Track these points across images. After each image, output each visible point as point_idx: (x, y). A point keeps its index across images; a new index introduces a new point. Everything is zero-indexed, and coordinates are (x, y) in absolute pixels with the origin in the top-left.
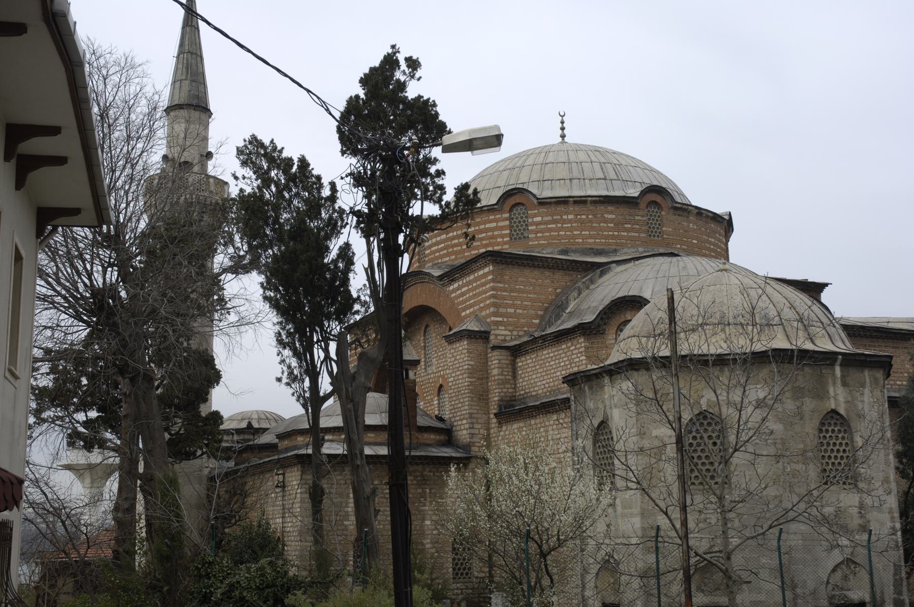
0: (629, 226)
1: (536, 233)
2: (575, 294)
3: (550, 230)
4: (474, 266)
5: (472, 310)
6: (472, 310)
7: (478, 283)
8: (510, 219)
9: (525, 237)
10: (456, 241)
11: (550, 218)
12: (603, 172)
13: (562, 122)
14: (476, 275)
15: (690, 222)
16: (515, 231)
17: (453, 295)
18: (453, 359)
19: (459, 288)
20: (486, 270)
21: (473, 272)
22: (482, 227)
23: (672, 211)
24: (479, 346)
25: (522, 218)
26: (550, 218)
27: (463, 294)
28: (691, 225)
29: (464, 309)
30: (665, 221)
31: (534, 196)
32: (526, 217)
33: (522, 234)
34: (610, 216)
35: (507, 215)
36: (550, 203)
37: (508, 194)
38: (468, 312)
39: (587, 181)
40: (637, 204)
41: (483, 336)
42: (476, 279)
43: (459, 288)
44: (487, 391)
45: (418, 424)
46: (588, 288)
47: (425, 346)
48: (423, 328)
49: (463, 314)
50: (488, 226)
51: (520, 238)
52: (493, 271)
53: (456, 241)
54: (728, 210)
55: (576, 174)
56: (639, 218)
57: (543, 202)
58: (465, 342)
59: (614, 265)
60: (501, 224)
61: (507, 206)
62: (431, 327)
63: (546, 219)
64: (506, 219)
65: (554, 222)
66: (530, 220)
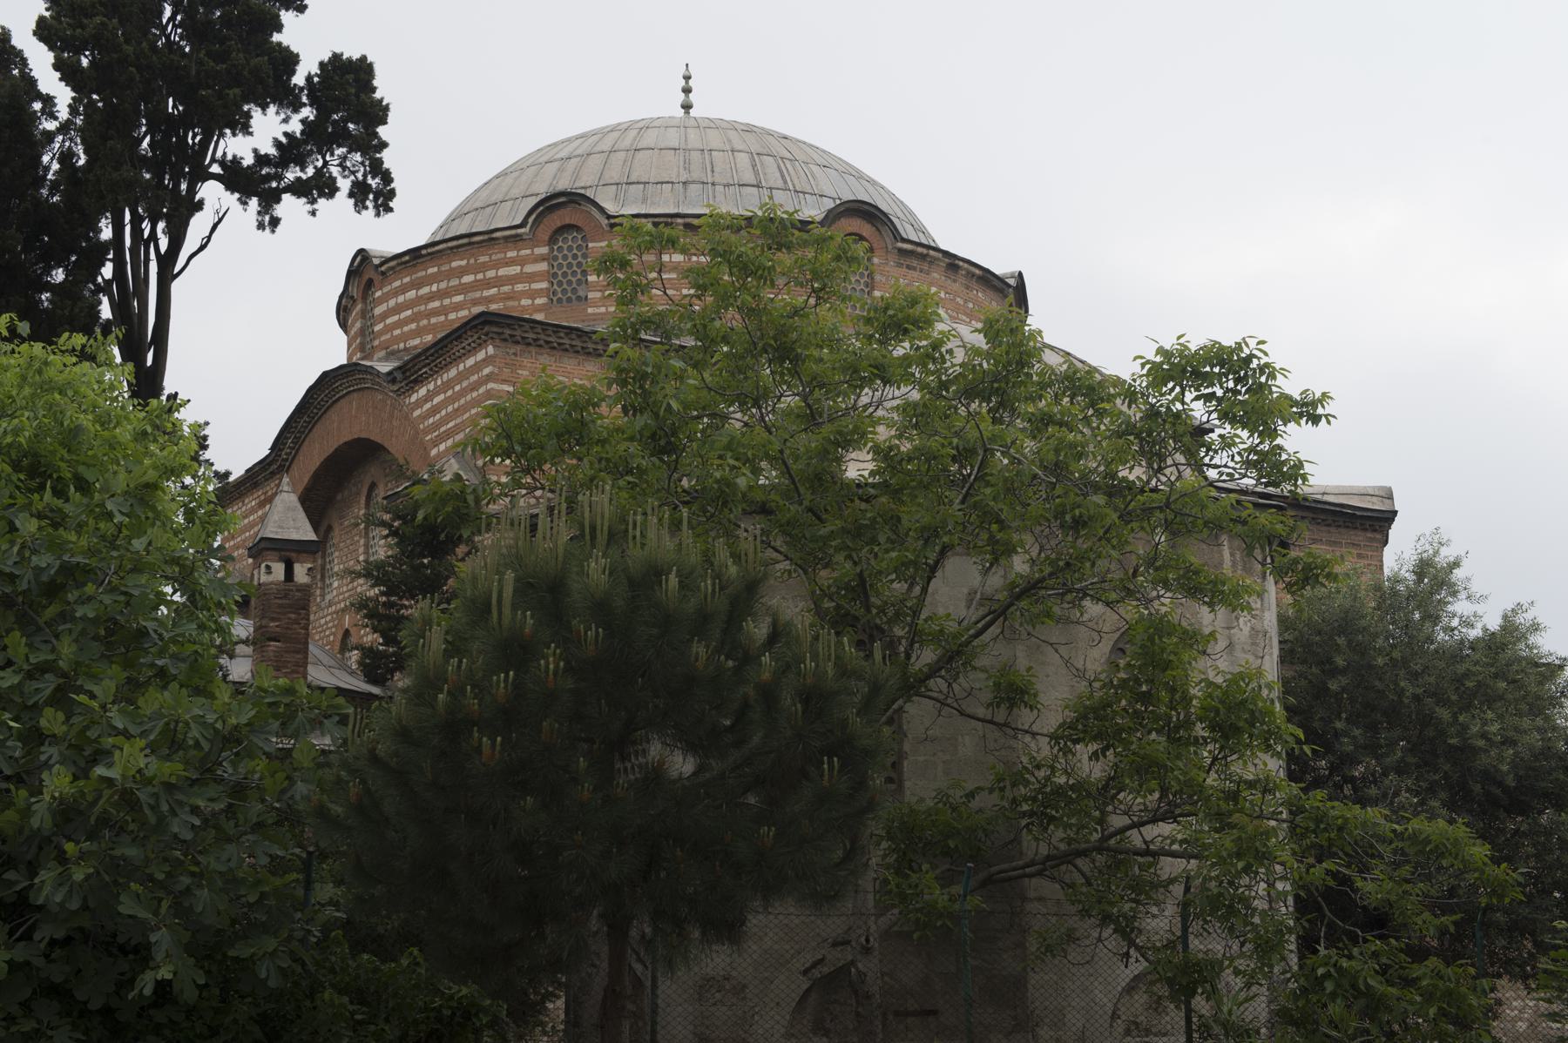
4: (457, 348)
6: (450, 442)
7: (465, 384)
9: (579, 298)
10: (436, 304)
12: (756, 173)
14: (461, 367)
15: (931, 284)
16: (560, 284)
17: (417, 413)
19: (429, 397)
20: (481, 355)
22: (491, 274)
25: (575, 257)
27: (435, 410)
29: (436, 443)
31: (602, 210)
33: (574, 291)
35: (544, 250)
37: (552, 203)
39: (719, 189)
43: (429, 397)
49: (434, 452)
50: (502, 272)
51: (569, 300)
53: (436, 304)
54: (1015, 269)
55: (696, 174)
60: (529, 269)
64: (543, 258)
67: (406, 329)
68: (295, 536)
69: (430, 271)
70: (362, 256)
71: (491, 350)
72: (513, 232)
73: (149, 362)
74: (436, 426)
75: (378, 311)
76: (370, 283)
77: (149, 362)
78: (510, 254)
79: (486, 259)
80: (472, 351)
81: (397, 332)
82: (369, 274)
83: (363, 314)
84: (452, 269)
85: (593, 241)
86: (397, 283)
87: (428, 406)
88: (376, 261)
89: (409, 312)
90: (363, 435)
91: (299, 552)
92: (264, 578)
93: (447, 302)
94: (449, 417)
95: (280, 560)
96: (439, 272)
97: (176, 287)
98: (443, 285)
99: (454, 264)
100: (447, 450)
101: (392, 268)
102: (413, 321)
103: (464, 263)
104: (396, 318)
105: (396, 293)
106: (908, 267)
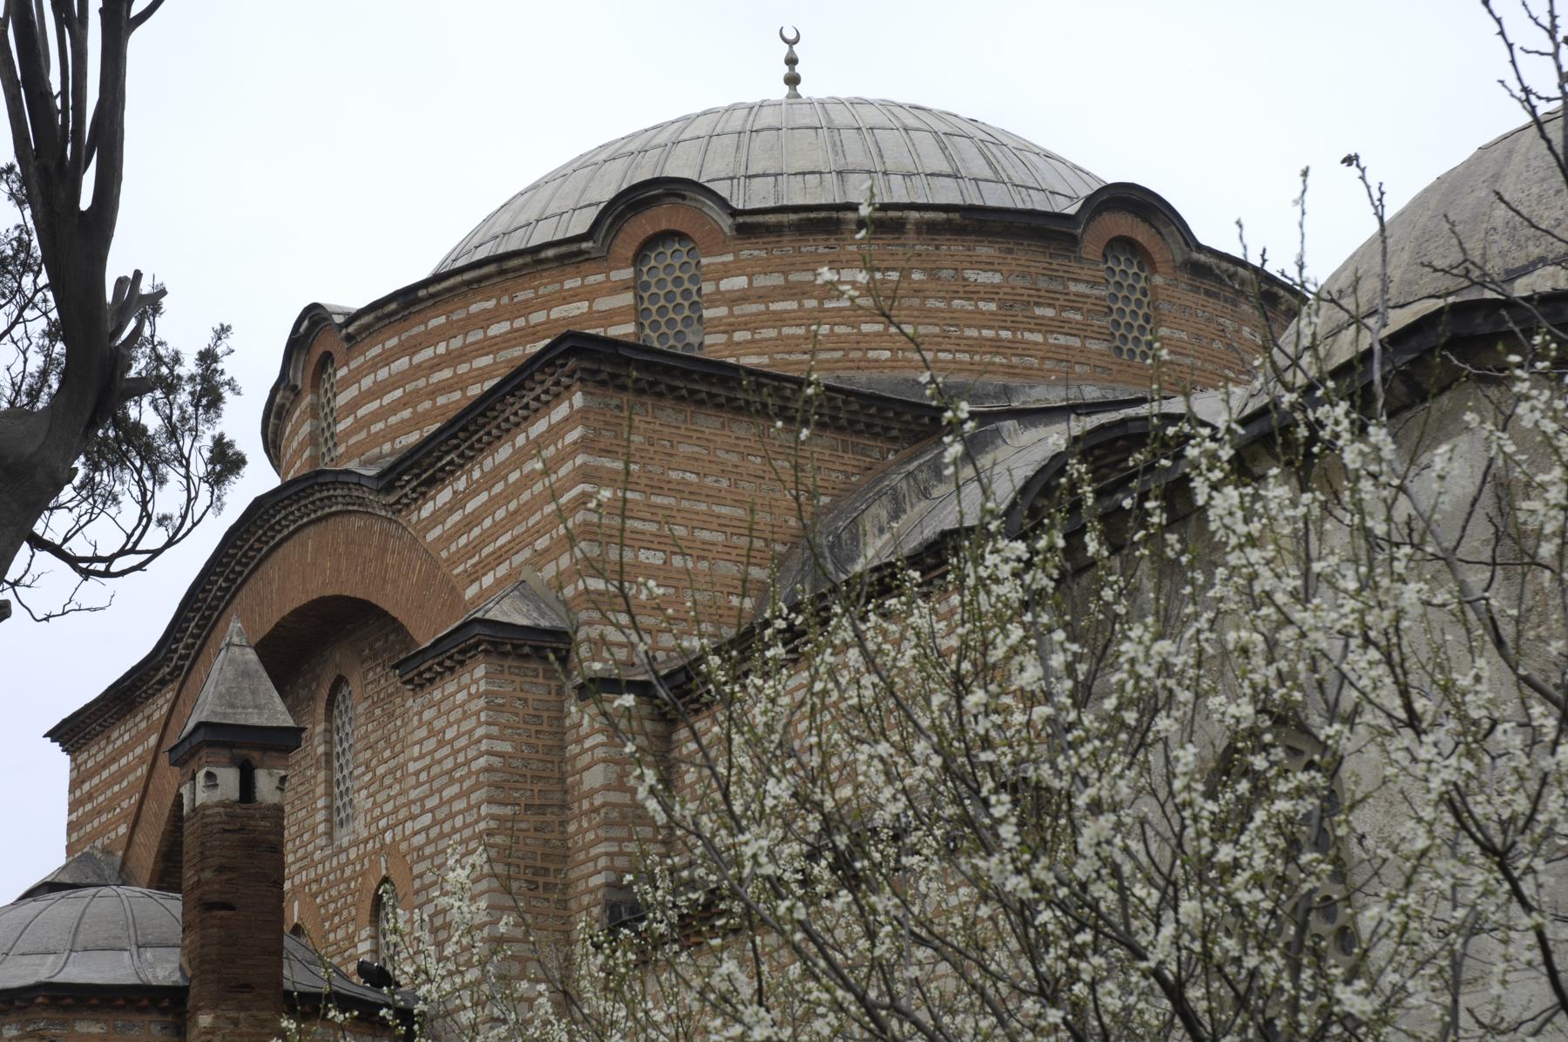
0: (1050, 312)
1: (730, 329)
2: (881, 511)
3: (780, 319)
4: (513, 407)
5: (502, 570)
6: (502, 570)
8: (638, 286)
10: (446, 373)
11: (777, 280)
12: (949, 159)
13: (791, 61)
14: (521, 440)
15: (1243, 321)
18: (430, 744)
20: (560, 412)
21: (507, 432)
23: (1185, 277)
24: (532, 687)
26: (777, 280)
28: (1246, 331)
29: (473, 576)
30: (1165, 307)
31: (722, 202)
32: (694, 279)
34: (983, 278)
35: (627, 273)
36: (777, 230)
38: (488, 580)
40: (1073, 241)
41: (541, 648)
42: (519, 458)
44: (562, 855)
45: (287, 985)
46: (925, 494)
47: (328, 755)
48: (324, 693)
49: (471, 592)
52: (584, 410)
53: (446, 373)
56: (1082, 288)
57: (752, 227)
58: (480, 671)
59: (1010, 424)
61: (626, 245)
62: (355, 681)
63: (762, 281)
64: (624, 287)
65: (793, 291)
66: (708, 288)
67: (393, 420)
68: (255, 720)
69: (433, 323)
70: (314, 316)
71: (578, 399)
72: (574, 247)
73: (85, 202)
74: (473, 548)
75: (342, 399)
76: (327, 359)
77: (85, 202)
78: (569, 284)
79: (530, 294)
80: (532, 414)
81: (377, 427)
82: (327, 342)
83: (314, 411)
84: (470, 317)
85: (707, 255)
86: (377, 350)
87: (457, 517)
88: (339, 319)
89: (398, 393)
90: (329, 592)
91: (265, 749)
92: (202, 796)
93: (463, 368)
94: (499, 528)
95: (232, 762)
96: (449, 323)
97: (137, 44)
98: (456, 343)
99: (474, 308)
100: (499, 583)
101: (366, 327)
102: (405, 406)
103: (491, 304)
104: (375, 405)
105: (374, 366)
106: (1207, 293)
